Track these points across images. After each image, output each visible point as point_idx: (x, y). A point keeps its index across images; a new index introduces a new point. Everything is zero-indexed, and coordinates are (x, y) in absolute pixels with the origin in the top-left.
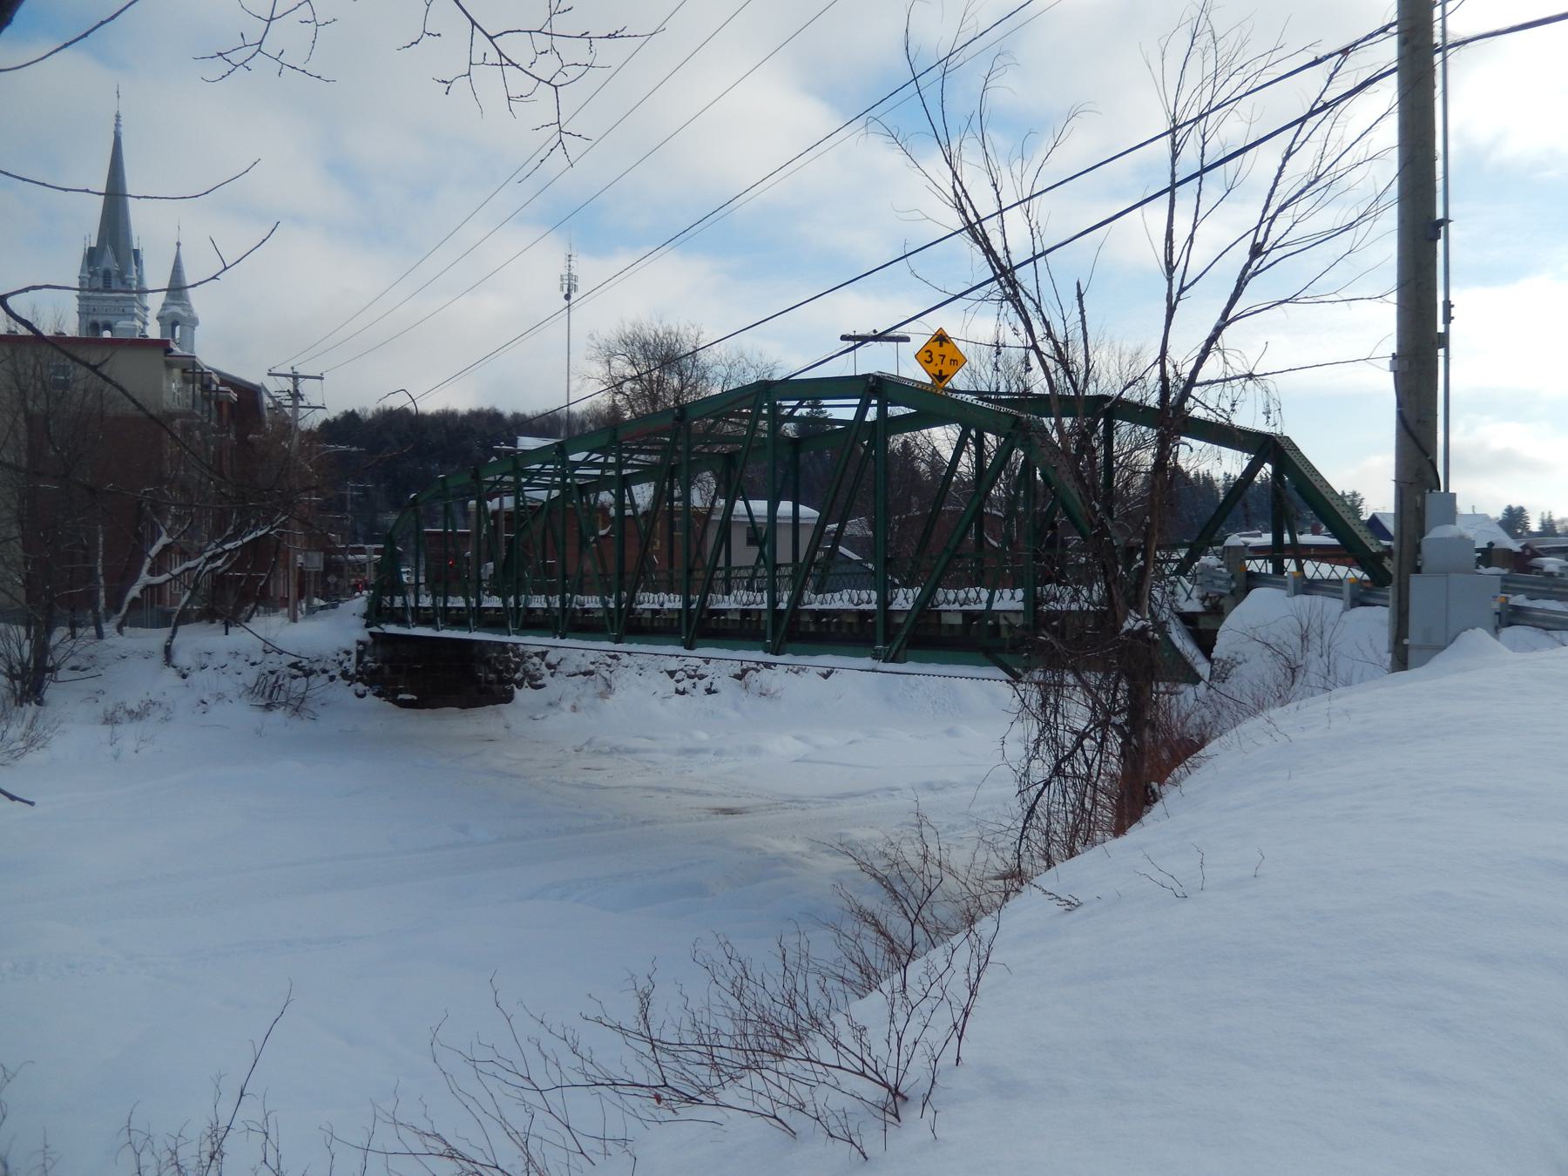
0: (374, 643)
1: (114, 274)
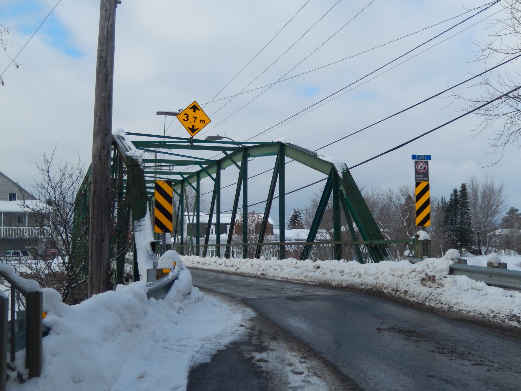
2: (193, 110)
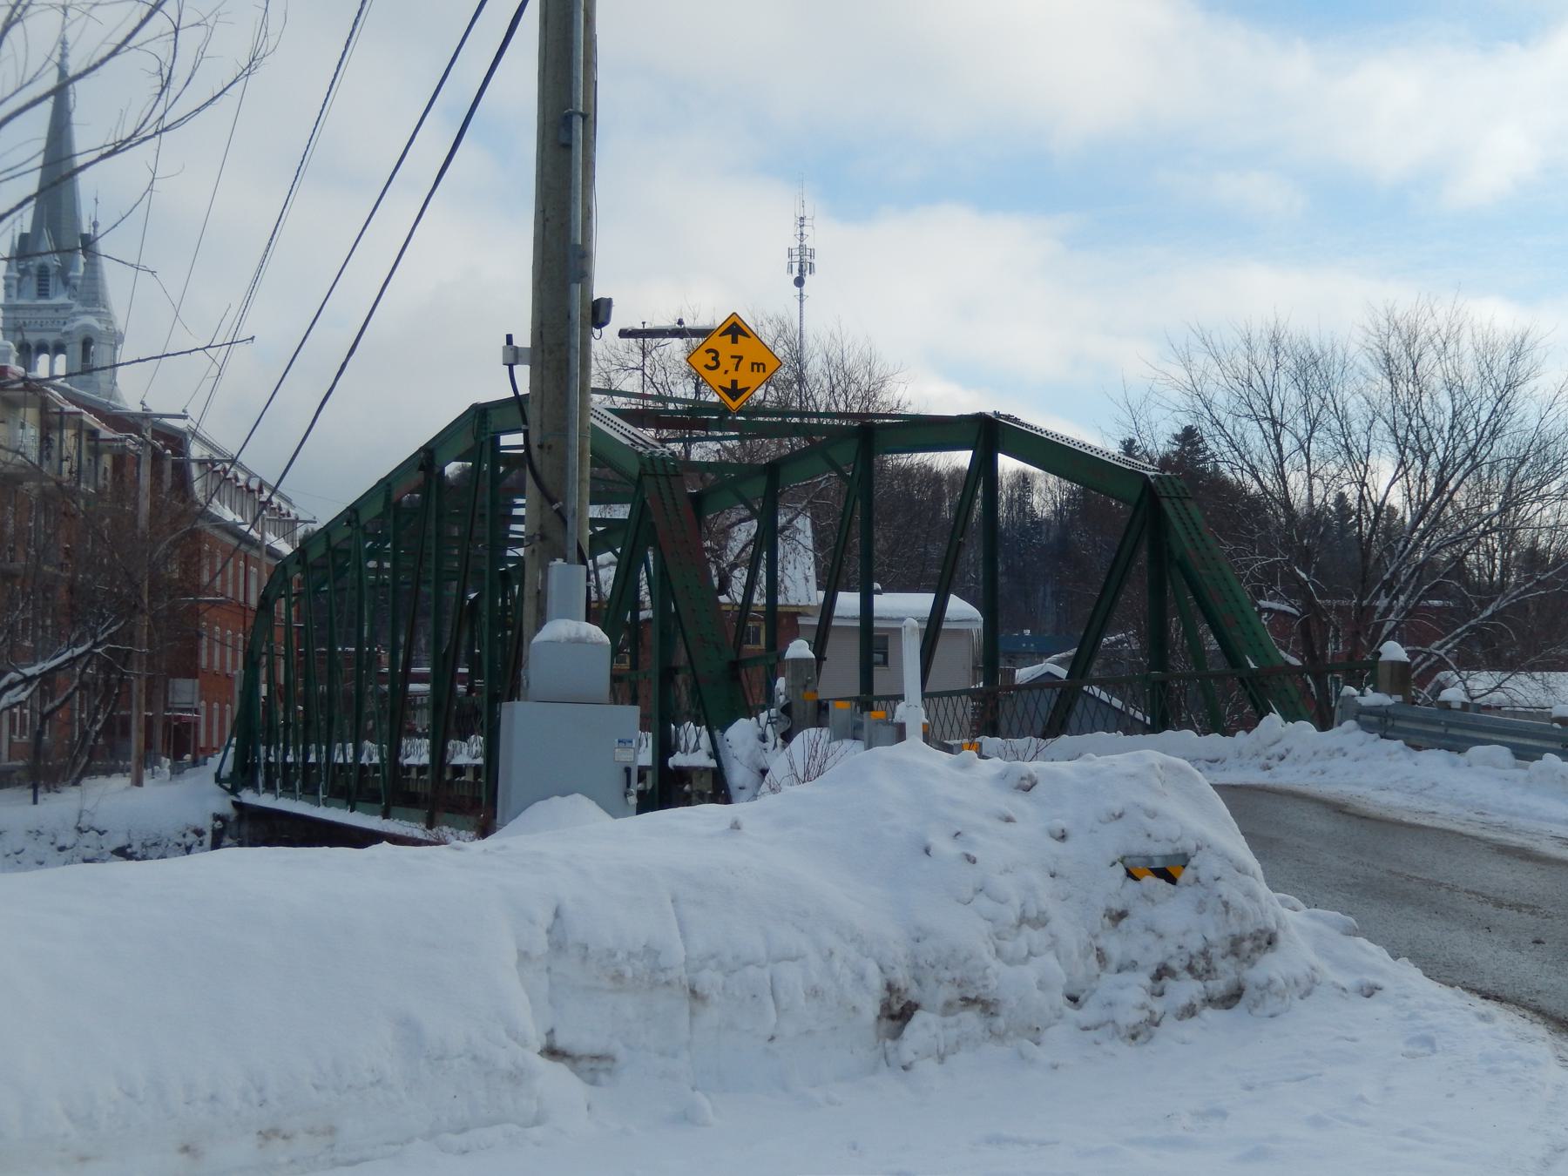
0: (240, 819)
1: (52, 271)
2: (729, 337)
